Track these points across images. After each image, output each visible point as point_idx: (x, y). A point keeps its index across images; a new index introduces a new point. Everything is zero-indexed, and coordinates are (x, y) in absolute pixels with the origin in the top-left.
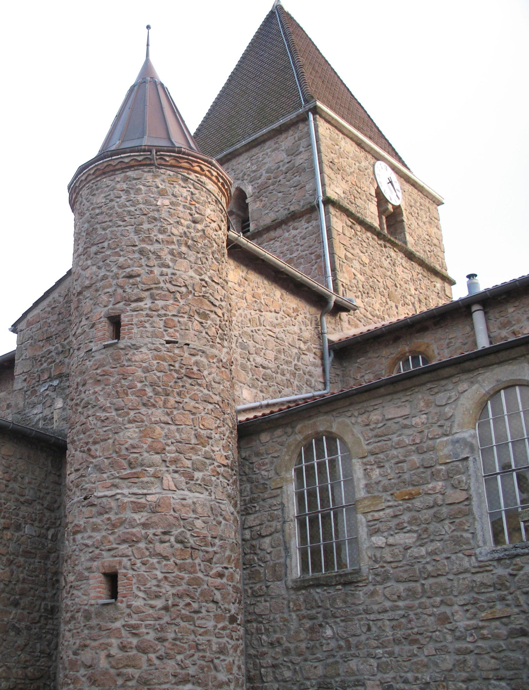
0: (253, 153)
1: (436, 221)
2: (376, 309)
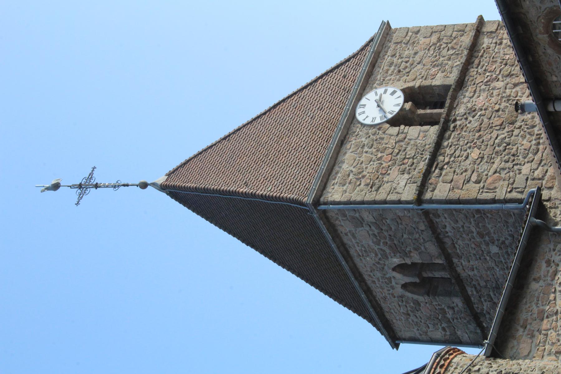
0: (355, 254)
1: (410, 34)
2: (529, 144)
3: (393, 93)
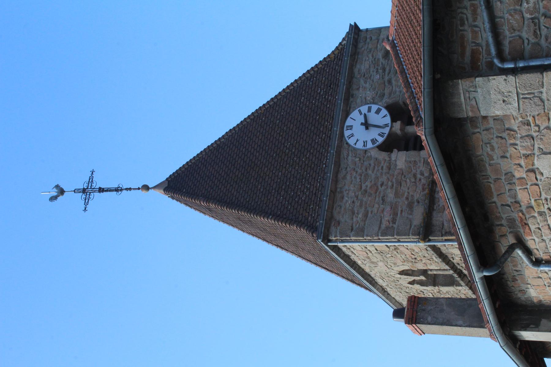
3: (378, 112)
